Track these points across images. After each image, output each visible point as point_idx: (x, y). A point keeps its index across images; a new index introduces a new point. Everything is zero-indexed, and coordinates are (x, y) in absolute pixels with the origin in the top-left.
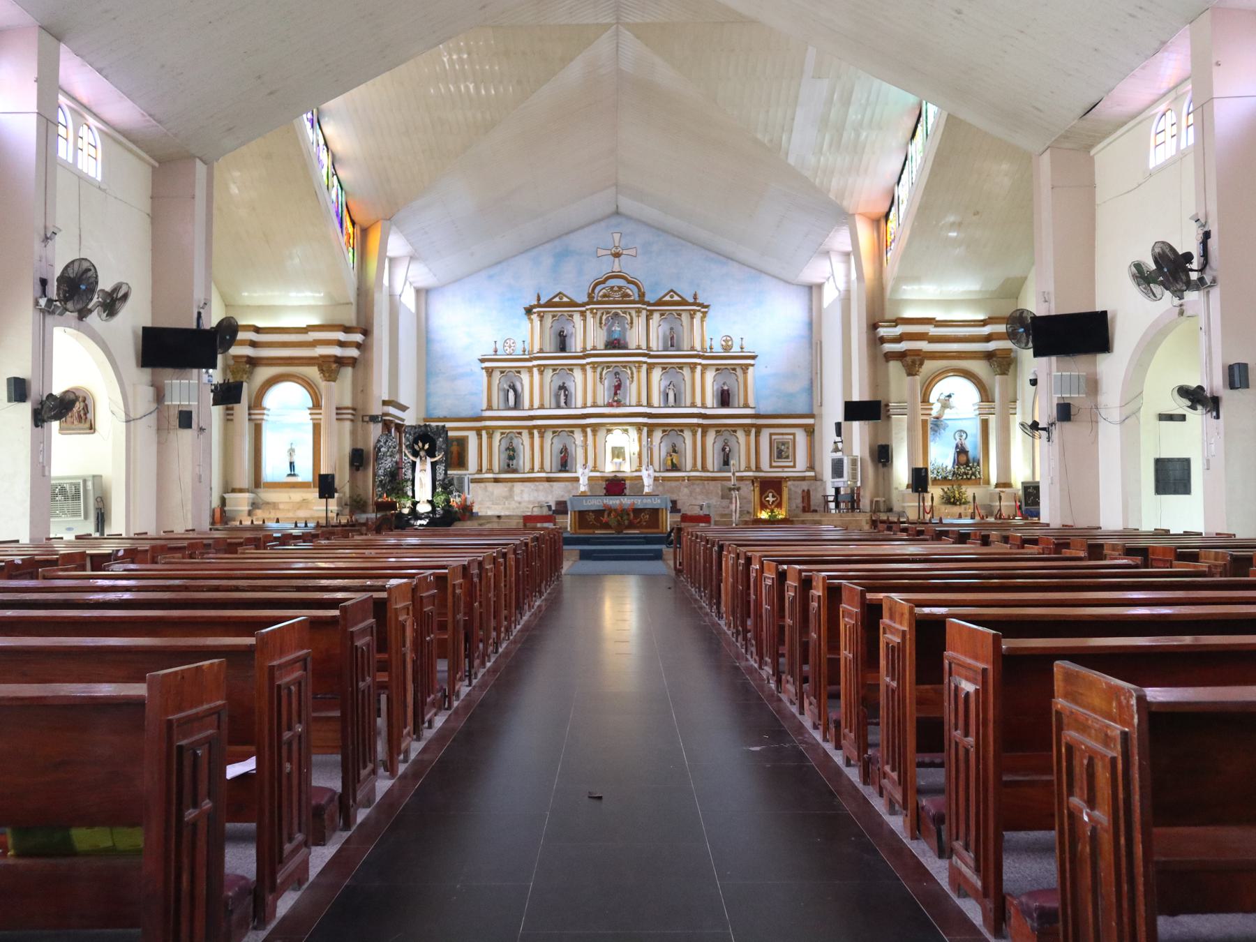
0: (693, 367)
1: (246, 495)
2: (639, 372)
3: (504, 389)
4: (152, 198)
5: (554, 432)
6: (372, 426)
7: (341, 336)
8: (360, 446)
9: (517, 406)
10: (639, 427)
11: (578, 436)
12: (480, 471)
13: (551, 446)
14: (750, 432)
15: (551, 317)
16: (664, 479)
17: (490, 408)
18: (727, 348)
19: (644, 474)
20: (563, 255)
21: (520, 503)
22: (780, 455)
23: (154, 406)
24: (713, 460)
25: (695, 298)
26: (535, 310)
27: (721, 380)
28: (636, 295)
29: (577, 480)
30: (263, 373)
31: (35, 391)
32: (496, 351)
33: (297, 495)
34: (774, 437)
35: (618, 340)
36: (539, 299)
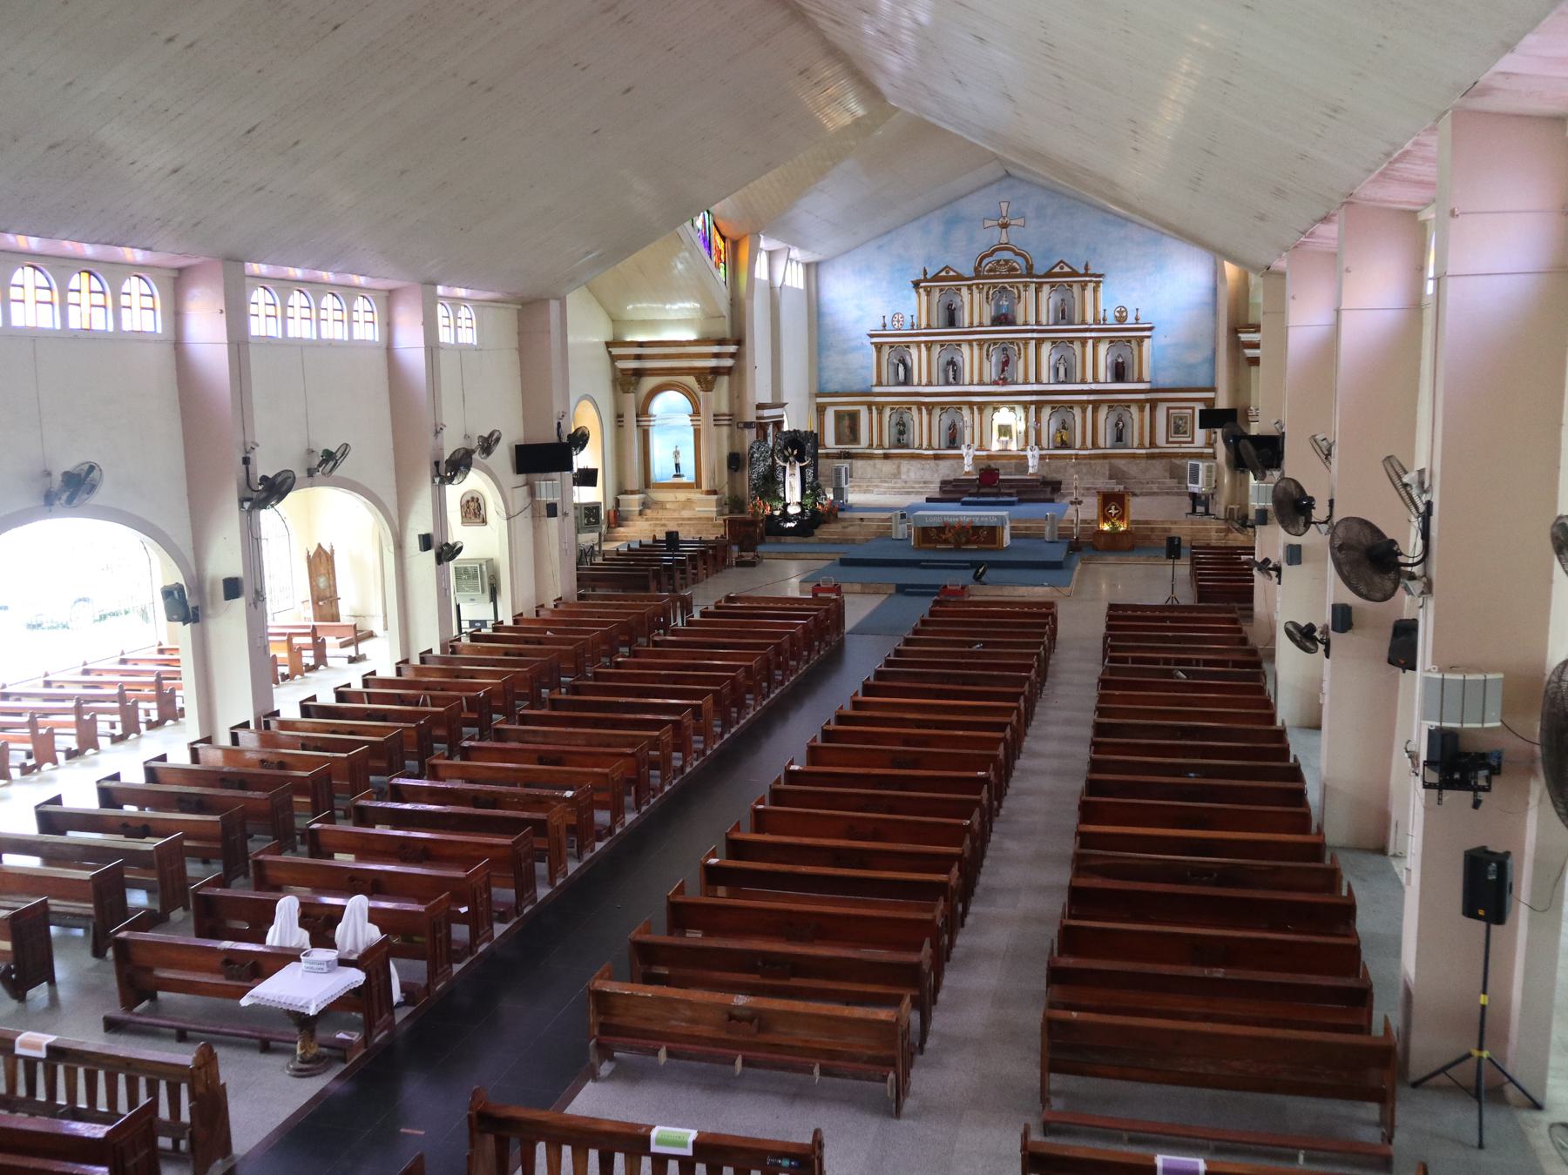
0: (1084, 341)
1: (637, 497)
2: (1026, 349)
3: (894, 364)
4: (518, 334)
5: (942, 409)
6: (747, 431)
7: (716, 349)
8: (737, 450)
9: (907, 382)
10: (1026, 405)
11: (966, 412)
12: (871, 446)
13: (940, 422)
14: (1144, 407)
15: (938, 291)
16: (1051, 457)
17: (879, 384)
18: (1121, 319)
19: (1029, 453)
20: (952, 222)
21: (906, 482)
22: (1178, 430)
23: (528, 500)
24: (1105, 436)
25: (1086, 268)
26: (922, 284)
27: (1115, 352)
28: (1024, 268)
29: (961, 457)
30: (649, 383)
31: (436, 541)
32: (884, 326)
33: (682, 495)
34: (1171, 411)
35: (1005, 316)
36: (925, 273)
